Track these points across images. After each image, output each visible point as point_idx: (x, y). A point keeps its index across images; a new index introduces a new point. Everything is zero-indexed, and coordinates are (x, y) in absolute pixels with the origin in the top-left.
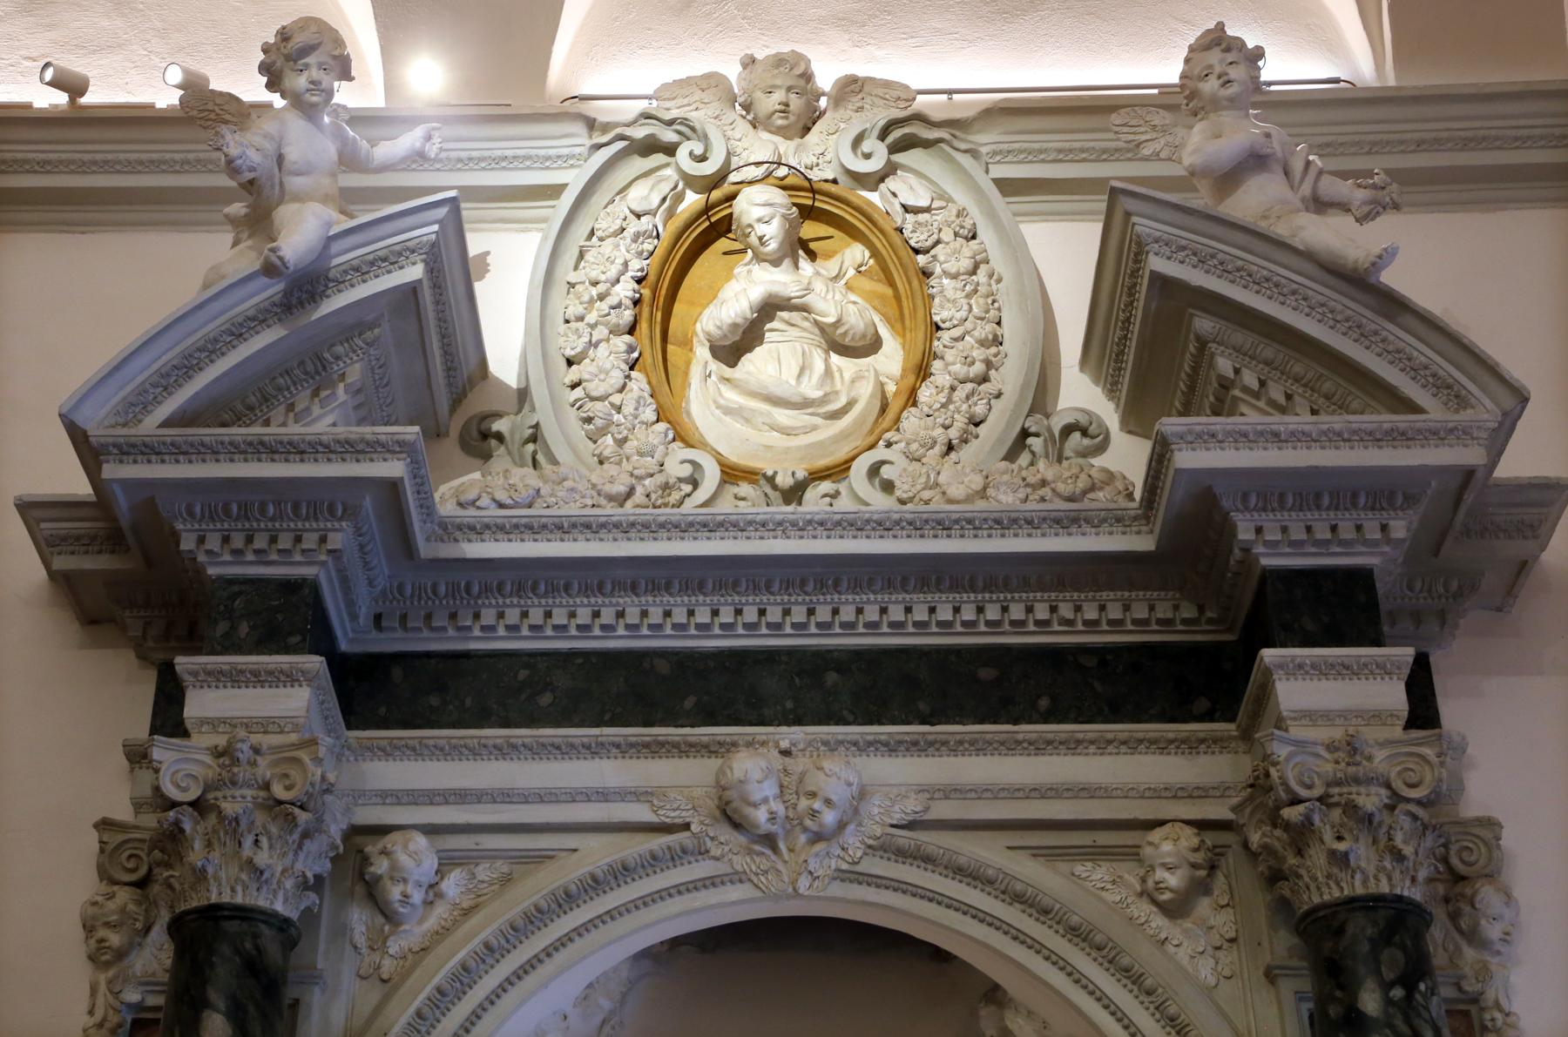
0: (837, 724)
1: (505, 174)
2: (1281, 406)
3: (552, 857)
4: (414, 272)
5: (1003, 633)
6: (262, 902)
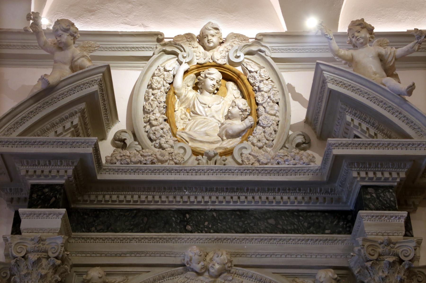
0: (224, 233)
2: (365, 131)
3: (140, 274)
4: (95, 88)
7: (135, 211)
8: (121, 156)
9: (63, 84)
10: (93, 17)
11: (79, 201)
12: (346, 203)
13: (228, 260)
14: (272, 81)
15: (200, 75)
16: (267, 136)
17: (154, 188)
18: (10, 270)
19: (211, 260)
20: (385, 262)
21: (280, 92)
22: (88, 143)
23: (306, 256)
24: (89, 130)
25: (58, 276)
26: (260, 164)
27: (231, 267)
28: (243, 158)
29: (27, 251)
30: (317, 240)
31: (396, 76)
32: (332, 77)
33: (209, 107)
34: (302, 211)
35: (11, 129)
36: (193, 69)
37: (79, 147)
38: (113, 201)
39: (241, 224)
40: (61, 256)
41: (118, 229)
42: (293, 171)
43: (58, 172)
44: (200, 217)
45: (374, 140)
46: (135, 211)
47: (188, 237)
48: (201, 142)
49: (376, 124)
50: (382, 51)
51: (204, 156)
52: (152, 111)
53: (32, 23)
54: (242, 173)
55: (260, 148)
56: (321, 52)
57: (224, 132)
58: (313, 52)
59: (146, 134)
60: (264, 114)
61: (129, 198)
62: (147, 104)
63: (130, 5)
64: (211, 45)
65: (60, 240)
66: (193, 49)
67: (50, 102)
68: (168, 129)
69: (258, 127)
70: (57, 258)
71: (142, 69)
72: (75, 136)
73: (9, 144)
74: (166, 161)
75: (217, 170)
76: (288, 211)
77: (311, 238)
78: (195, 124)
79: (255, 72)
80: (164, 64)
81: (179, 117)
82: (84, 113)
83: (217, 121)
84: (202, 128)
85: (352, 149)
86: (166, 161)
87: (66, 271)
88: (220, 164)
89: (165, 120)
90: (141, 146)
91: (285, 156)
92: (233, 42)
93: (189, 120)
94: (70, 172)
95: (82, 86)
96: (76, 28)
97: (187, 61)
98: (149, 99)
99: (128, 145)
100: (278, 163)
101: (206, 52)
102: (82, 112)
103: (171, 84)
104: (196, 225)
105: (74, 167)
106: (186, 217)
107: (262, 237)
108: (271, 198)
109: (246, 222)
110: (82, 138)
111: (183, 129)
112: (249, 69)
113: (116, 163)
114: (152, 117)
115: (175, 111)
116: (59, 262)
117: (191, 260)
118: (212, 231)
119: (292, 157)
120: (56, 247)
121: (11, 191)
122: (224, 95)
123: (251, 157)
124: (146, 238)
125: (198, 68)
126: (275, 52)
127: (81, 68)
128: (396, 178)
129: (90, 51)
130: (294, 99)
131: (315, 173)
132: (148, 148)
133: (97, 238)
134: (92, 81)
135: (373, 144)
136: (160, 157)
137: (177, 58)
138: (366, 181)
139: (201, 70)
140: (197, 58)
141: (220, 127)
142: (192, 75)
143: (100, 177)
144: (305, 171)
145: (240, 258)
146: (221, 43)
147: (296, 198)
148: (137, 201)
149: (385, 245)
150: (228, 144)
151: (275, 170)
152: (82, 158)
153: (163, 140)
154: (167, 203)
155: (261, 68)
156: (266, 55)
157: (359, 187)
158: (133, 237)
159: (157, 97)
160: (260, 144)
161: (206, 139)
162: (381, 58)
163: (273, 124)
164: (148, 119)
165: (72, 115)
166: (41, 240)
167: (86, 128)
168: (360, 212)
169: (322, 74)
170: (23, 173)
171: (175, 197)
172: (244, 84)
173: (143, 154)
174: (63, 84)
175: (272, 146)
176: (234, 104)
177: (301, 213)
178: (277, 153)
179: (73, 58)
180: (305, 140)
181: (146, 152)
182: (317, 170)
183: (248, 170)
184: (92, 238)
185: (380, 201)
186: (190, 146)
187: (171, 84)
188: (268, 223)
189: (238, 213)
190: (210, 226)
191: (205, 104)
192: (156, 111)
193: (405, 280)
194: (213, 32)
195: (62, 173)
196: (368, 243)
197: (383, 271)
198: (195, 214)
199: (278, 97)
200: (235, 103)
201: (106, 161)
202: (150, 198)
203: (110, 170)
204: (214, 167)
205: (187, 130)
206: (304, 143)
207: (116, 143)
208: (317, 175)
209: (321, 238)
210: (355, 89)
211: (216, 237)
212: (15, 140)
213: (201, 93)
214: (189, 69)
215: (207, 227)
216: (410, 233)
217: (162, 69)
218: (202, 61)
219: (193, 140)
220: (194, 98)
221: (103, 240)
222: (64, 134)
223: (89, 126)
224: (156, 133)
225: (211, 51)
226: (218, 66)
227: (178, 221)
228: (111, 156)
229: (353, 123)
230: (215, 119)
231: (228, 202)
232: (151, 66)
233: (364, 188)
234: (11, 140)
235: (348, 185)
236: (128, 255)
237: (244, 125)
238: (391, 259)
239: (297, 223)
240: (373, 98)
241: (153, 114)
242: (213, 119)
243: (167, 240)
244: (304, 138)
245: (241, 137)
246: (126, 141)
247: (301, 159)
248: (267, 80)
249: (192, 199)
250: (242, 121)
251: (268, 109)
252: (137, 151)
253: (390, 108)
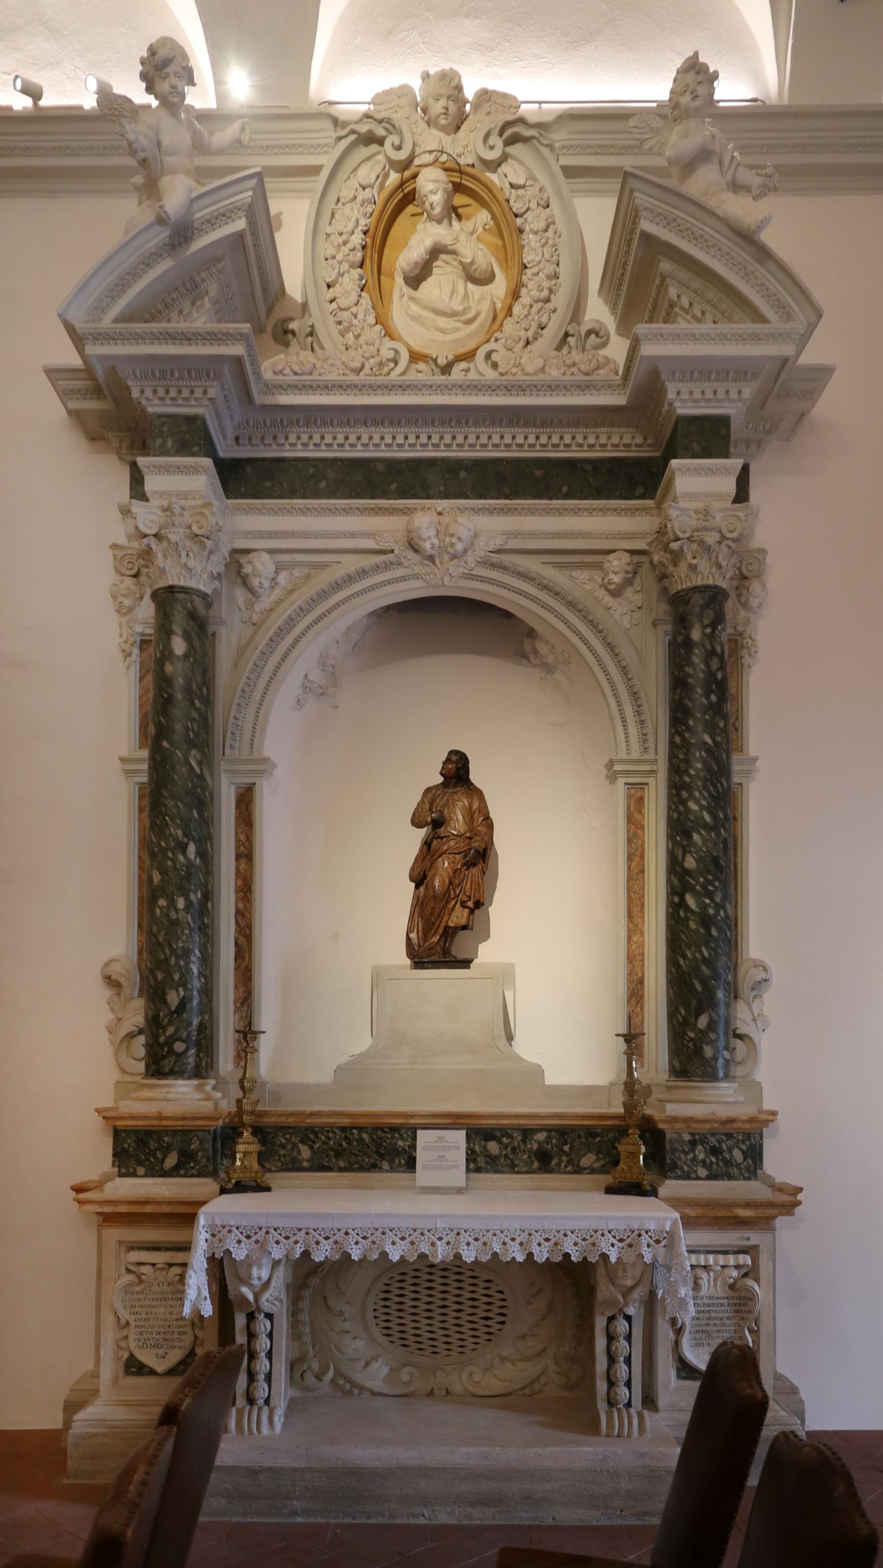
4: (240, 224)
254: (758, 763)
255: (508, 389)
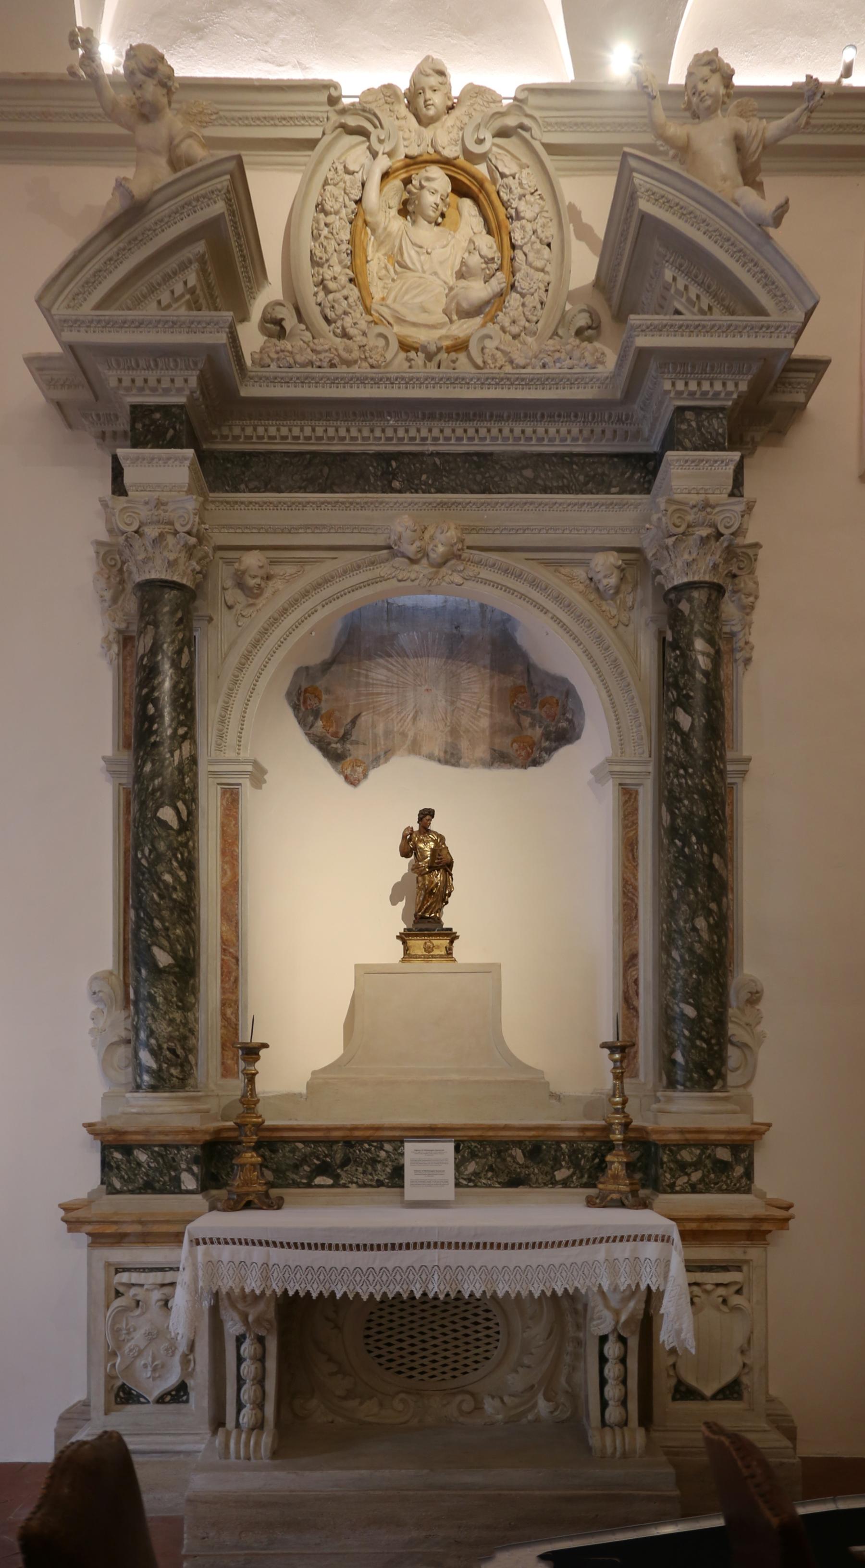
0: (453, 493)
1: (256, 129)
4: (219, 207)
5: (313, 444)
6: (696, 579)
7: (308, 456)
8: (277, 353)
9: (159, 198)
10: (201, 43)
11: (215, 437)
12: (648, 440)
13: (458, 538)
14: (541, 198)
15: (411, 182)
16: (527, 313)
17: (337, 414)
18: (121, 554)
19: (432, 538)
20: (694, 536)
21: (554, 223)
22: (217, 323)
23: (578, 530)
24: (218, 300)
25: (195, 564)
26: (513, 368)
27: (462, 549)
28: (486, 356)
29: (140, 522)
30: (596, 505)
31: (758, 186)
32: (648, 186)
33: (428, 253)
34: (578, 455)
35: (78, 294)
36: (397, 170)
37: (203, 332)
38: (270, 438)
39: (479, 477)
40: (195, 530)
41: (282, 487)
42: (568, 380)
43: (172, 381)
44: (414, 465)
45: (706, 318)
46: (308, 456)
47: (395, 500)
48: (414, 325)
49: (714, 287)
50: (744, 126)
51: (419, 353)
52: (327, 260)
53: (83, 55)
54: (483, 384)
55: (515, 337)
56: (633, 131)
57: (453, 305)
58: (619, 132)
59: (318, 308)
60: (524, 268)
61: (296, 431)
62: (317, 245)
63: (272, 15)
64: (432, 112)
65: (191, 504)
66: (397, 123)
67: (140, 238)
68: (356, 298)
69: (514, 294)
70: (189, 533)
71: (303, 168)
72: (192, 310)
73: (79, 326)
74: (356, 362)
75: (441, 379)
76: (555, 455)
77: (587, 501)
78: (404, 288)
79: (511, 175)
80: (343, 158)
81: (375, 274)
82: (205, 263)
83: (442, 283)
84: (415, 296)
85: (668, 336)
86: (356, 362)
87: (206, 556)
88: (447, 368)
89: (351, 280)
90: (311, 332)
91: (555, 351)
92: (472, 105)
93: (393, 280)
94: (193, 382)
95: (194, 203)
96: (170, 67)
97: (387, 150)
98: (320, 235)
99: (288, 332)
100: (544, 366)
101: (423, 129)
102: (201, 260)
103: (358, 202)
104: (408, 481)
105: (198, 372)
106: (391, 466)
107: (511, 500)
108: (529, 431)
109: (487, 475)
110: (206, 314)
111: (383, 299)
112: (500, 170)
113: (269, 366)
114: (328, 274)
115: (367, 262)
116: (193, 540)
117: (400, 538)
118: (433, 490)
119: (567, 354)
120: (186, 516)
121: (99, 419)
122: (455, 228)
123: (499, 354)
124: (329, 503)
125: (407, 166)
126: (549, 131)
127: (189, 163)
128: (732, 393)
129: (204, 124)
130: (579, 237)
131: (603, 383)
132: (324, 337)
133: (251, 503)
134: (213, 192)
135: (704, 327)
136: (345, 355)
137: (368, 144)
138: (684, 399)
139: (413, 172)
140: (406, 143)
141: (447, 295)
142: (396, 183)
143: (246, 391)
144: (587, 380)
145: (476, 536)
146: (451, 108)
147: (569, 432)
148: (310, 438)
149: (699, 510)
150: (462, 328)
151: (538, 380)
152: (211, 353)
153: (348, 321)
154: (359, 442)
155: (522, 166)
156: (532, 136)
157: (671, 409)
158: (307, 500)
159: (334, 232)
160: (515, 329)
161: (423, 318)
162: (739, 144)
163: (539, 288)
164: (321, 277)
165: (184, 266)
166: (160, 504)
167: (212, 296)
168: (669, 453)
169: (631, 178)
170: (113, 383)
171: (372, 431)
172: (491, 203)
173: (314, 347)
174: (159, 198)
175: (535, 334)
176: (472, 247)
177: (575, 459)
178: (543, 346)
179: (171, 139)
180: (592, 320)
181: (321, 344)
182: (607, 378)
183: (493, 379)
184: (242, 503)
185: (702, 434)
186: (396, 334)
187: (358, 202)
188: (522, 476)
189: (475, 458)
190: (430, 482)
191: (421, 247)
192: (334, 260)
193: (721, 565)
194: (434, 80)
195: (179, 383)
196: (674, 507)
197: (690, 552)
198: (406, 460)
199: (550, 232)
200: (474, 243)
201: (253, 362)
202: (331, 432)
203: (261, 379)
204: (437, 373)
205: (389, 302)
206: (589, 327)
207: (266, 328)
208: (606, 388)
209: (604, 501)
210: (685, 212)
211: (439, 500)
212: (90, 318)
213: (414, 222)
214: (390, 167)
215: (426, 483)
216: (740, 491)
217: (340, 168)
218: (414, 151)
219: (401, 320)
220: (400, 233)
221: (261, 505)
222: (175, 306)
223: (217, 292)
224: (336, 306)
225: (431, 127)
226: (445, 163)
227: (379, 473)
228: (261, 352)
229: (675, 285)
230: (439, 278)
231: (459, 439)
232: (319, 162)
233: (680, 410)
234: (81, 318)
235: (655, 407)
236: (300, 531)
237: (489, 289)
238: (704, 532)
239: (568, 476)
240: (715, 231)
241: (329, 266)
242: (435, 278)
243: (363, 506)
244: (591, 317)
245: (482, 316)
246: (284, 323)
247: (583, 357)
248: (532, 194)
249: (401, 433)
250: (485, 282)
251: (531, 256)
252: (304, 342)
253: (740, 254)
254: (751, 763)
255: (484, 382)
